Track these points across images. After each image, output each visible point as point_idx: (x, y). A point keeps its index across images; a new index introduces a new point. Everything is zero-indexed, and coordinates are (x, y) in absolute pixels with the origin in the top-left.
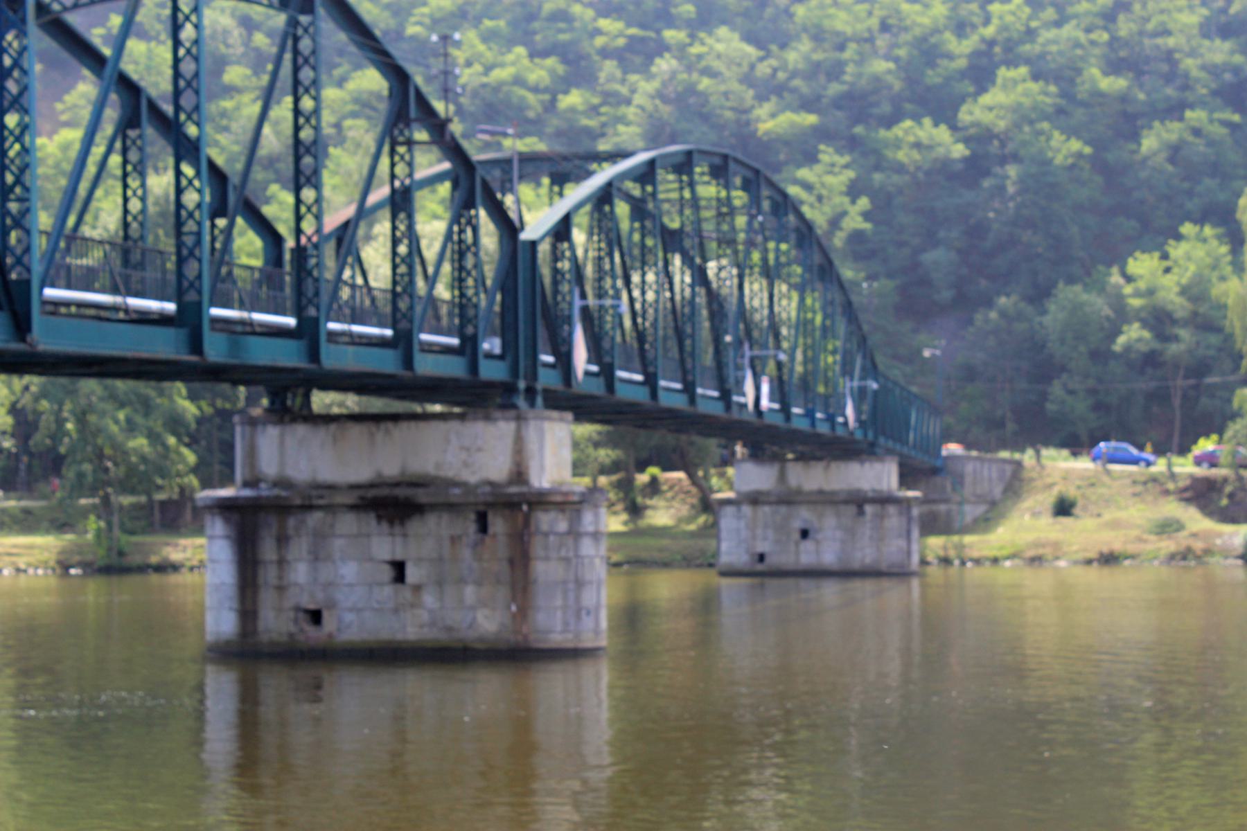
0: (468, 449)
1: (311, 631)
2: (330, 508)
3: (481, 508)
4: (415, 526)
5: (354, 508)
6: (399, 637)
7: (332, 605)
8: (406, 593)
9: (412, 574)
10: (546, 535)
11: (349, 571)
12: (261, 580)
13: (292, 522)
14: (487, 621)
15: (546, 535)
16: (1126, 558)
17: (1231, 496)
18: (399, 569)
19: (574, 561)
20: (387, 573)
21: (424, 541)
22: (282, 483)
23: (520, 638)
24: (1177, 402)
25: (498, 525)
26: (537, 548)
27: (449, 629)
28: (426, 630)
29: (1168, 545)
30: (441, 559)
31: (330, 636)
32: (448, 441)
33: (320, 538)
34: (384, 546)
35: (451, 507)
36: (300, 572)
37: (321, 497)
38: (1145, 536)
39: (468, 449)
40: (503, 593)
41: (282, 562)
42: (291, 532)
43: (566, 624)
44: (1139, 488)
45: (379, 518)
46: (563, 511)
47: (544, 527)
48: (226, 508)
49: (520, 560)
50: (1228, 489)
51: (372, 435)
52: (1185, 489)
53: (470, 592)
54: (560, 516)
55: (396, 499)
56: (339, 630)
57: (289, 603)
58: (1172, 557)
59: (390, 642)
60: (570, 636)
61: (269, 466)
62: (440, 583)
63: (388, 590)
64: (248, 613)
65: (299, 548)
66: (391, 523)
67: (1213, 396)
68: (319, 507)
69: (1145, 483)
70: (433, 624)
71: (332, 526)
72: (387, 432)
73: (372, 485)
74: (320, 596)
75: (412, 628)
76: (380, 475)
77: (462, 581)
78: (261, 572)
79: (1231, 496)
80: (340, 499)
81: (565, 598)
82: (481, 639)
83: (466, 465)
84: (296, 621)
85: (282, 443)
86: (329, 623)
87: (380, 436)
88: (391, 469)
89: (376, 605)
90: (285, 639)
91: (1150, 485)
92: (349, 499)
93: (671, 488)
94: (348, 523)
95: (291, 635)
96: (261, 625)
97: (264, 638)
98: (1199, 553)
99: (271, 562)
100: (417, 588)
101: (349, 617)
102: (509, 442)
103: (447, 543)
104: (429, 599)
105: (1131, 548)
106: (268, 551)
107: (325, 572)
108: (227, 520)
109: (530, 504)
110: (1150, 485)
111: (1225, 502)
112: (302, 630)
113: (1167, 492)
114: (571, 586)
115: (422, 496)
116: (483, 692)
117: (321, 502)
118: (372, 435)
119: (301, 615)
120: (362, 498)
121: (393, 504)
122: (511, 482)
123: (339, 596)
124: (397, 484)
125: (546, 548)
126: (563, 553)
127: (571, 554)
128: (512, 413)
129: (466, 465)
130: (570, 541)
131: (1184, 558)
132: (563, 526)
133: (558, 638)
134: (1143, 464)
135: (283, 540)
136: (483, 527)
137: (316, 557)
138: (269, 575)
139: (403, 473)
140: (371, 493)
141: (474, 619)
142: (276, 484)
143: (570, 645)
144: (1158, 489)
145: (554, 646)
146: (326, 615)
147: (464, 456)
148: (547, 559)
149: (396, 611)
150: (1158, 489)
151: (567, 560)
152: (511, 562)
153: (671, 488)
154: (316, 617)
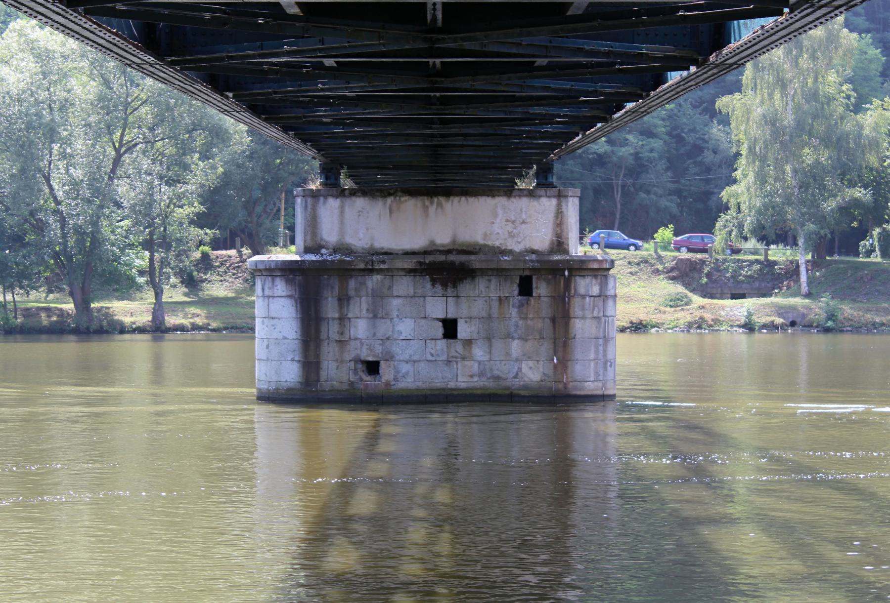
0: (513, 222)
1: (368, 379)
2: (389, 273)
3: (527, 273)
4: (466, 288)
5: (410, 272)
6: (452, 385)
7: (390, 357)
8: (457, 347)
9: (463, 331)
10: (584, 297)
11: (406, 327)
12: (323, 335)
13: (352, 284)
14: (533, 373)
15: (584, 297)
16: (653, 327)
17: (708, 275)
18: (450, 328)
19: (603, 319)
20: (439, 330)
21: (473, 304)
22: (341, 248)
23: (561, 386)
24: (618, 197)
25: (541, 289)
26: (576, 308)
27: (498, 378)
28: (476, 379)
29: (684, 316)
30: (490, 317)
31: (388, 384)
32: (496, 215)
33: (379, 299)
34: (438, 306)
35: (500, 273)
36: (360, 328)
37: (384, 262)
38: (663, 308)
39: (513, 222)
40: (546, 347)
41: (343, 319)
42: (352, 293)
43: (597, 374)
44: (634, 269)
45: (434, 282)
46: (596, 276)
47: (582, 291)
48: (287, 270)
49: (561, 319)
50: (706, 270)
51: (426, 209)
52: (672, 269)
53: (516, 347)
54: (594, 281)
55: (452, 263)
56: (396, 379)
57: (348, 357)
58: (690, 326)
59: (444, 389)
60: (600, 384)
61: (329, 233)
62: (489, 339)
63: (442, 344)
64: (310, 364)
65: (359, 308)
66: (445, 286)
67: (648, 192)
68: (379, 271)
69: (638, 264)
70: (481, 374)
71: (390, 288)
72: (440, 205)
73: (425, 253)
74: (378, 349)
75: (463, 378)
76: (432, 243)
77: (509, 336)
78: (324, 329)
79: (708, 275)
80: (400, 264)
81: (597, 352)
82: (526, 387)
83: (511, 235)
84: (355, 371)
85: (342, 213)
86: (386, 373)
87: (432, 209)
88: (443, 239)
89: (430, 358)
90: (345, 387)
91: (642, 265)
92: (409, 264)
93: (222, 264)
94: (404, 285)
95: (352, 384)
96: (323, 375)
97: (327, 386)
98: (710, 322)
99: (333, 319)
100: (468, 343)
101: (405, 368)
102: (550, 216)
103: (495, 304)
104: (479, 352)
105: (655, 318)
106: (330, 309)
107: (383, 328)
108: (289, 282)
109: (570, 270)
110: (642, 265)
111: (705, 280)
112: (361, 379)
113: (657, 272)
114: (601, 341)
115: (475, 262)
116: (528, 432)
117: (382, 266)
118: (426, 209)
119: (360, 366)
120: (420, 263)
121: (448, 269)
122: (552, 252)
123: (396, 349)
124: (449, 252)
125: (583, 309)
126: (595, 314)
127: (601, 314)
128: (554, 191)
129: (511, 235)
130: (600, 302)
131: (699, 327)
132: (595, 290)
133: (591, 387)
134: (632, 248)
135: (344, 300)
136: (526, 288)
137: (376, 314)
138: (331, 330)
139: (454, 242)
140: (428, 259)
141: (520, 369)
142: (335, 251)
143: (599, 392)
144: (649, 269)
145: (589, 393)
146: (383, 365)
147: (510, 227)
148: (584, 318)
149: (448, 362)
150: (649, 269)
151: (597, 318)
152: (553, 320)
153: (222, 264)
154: (373, 368)
